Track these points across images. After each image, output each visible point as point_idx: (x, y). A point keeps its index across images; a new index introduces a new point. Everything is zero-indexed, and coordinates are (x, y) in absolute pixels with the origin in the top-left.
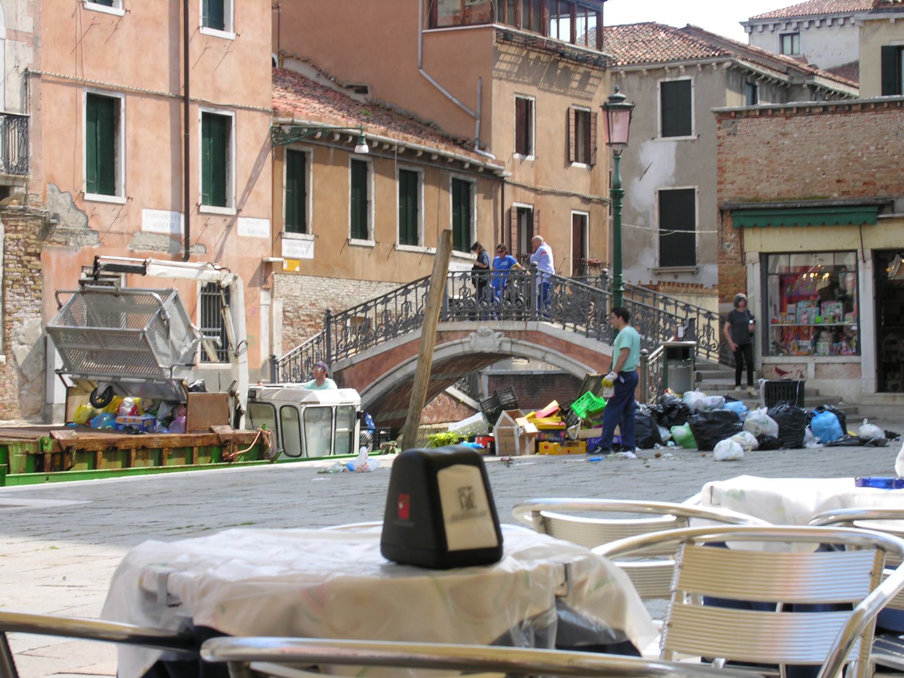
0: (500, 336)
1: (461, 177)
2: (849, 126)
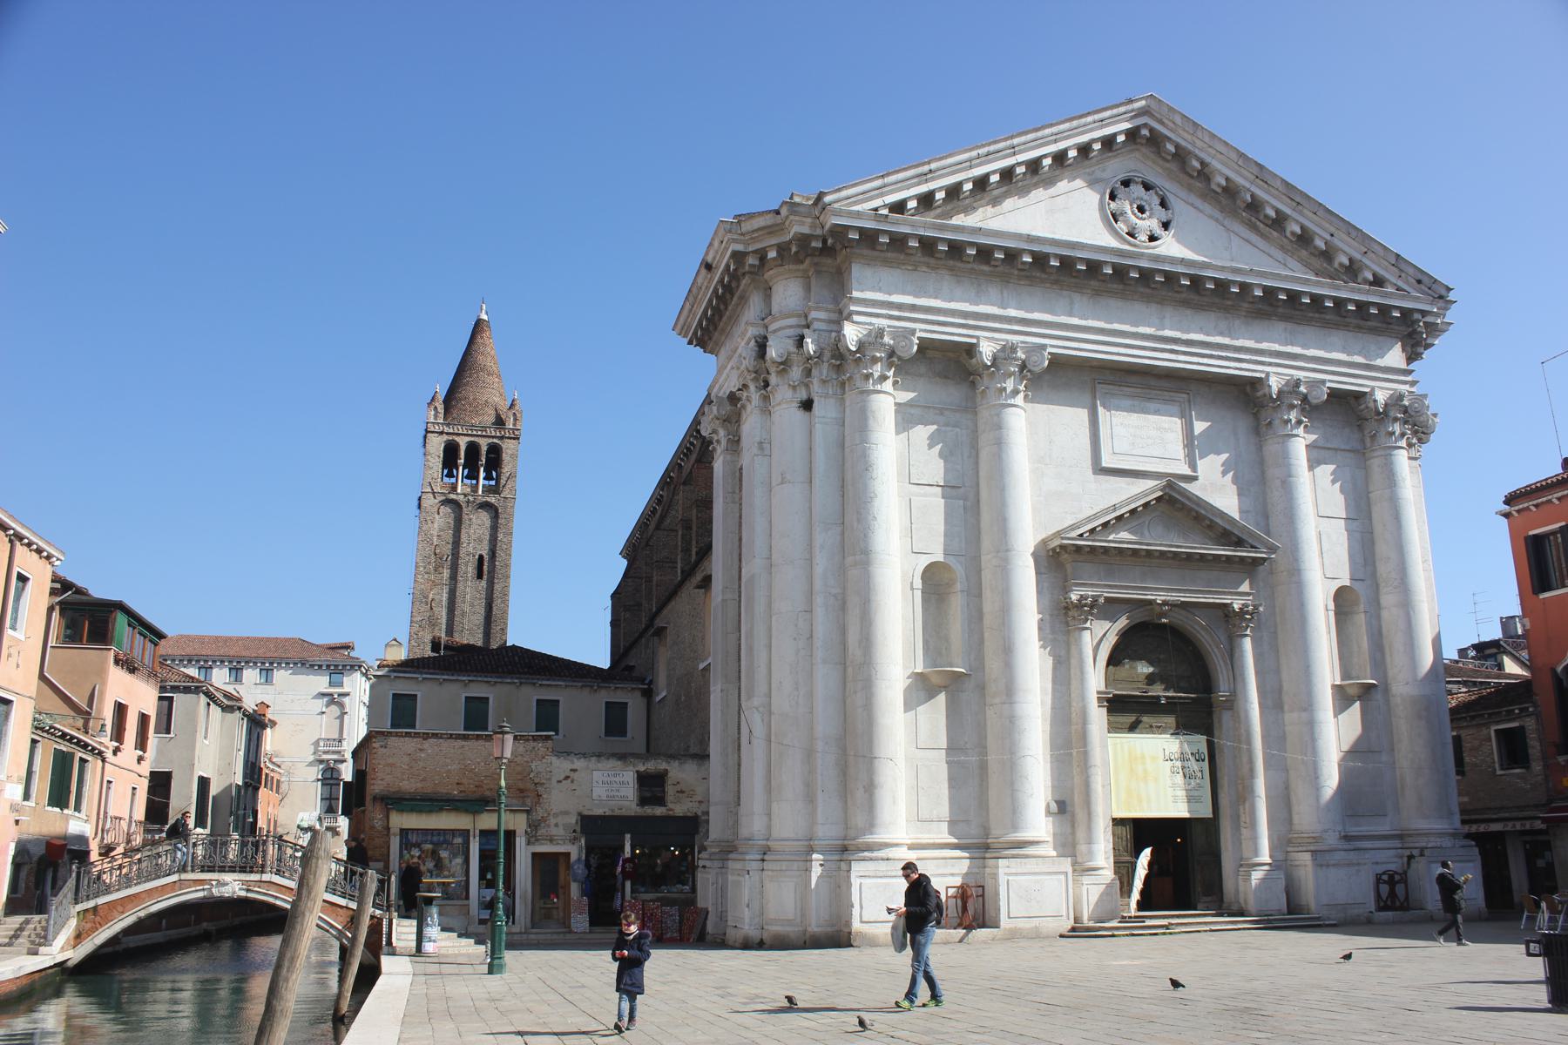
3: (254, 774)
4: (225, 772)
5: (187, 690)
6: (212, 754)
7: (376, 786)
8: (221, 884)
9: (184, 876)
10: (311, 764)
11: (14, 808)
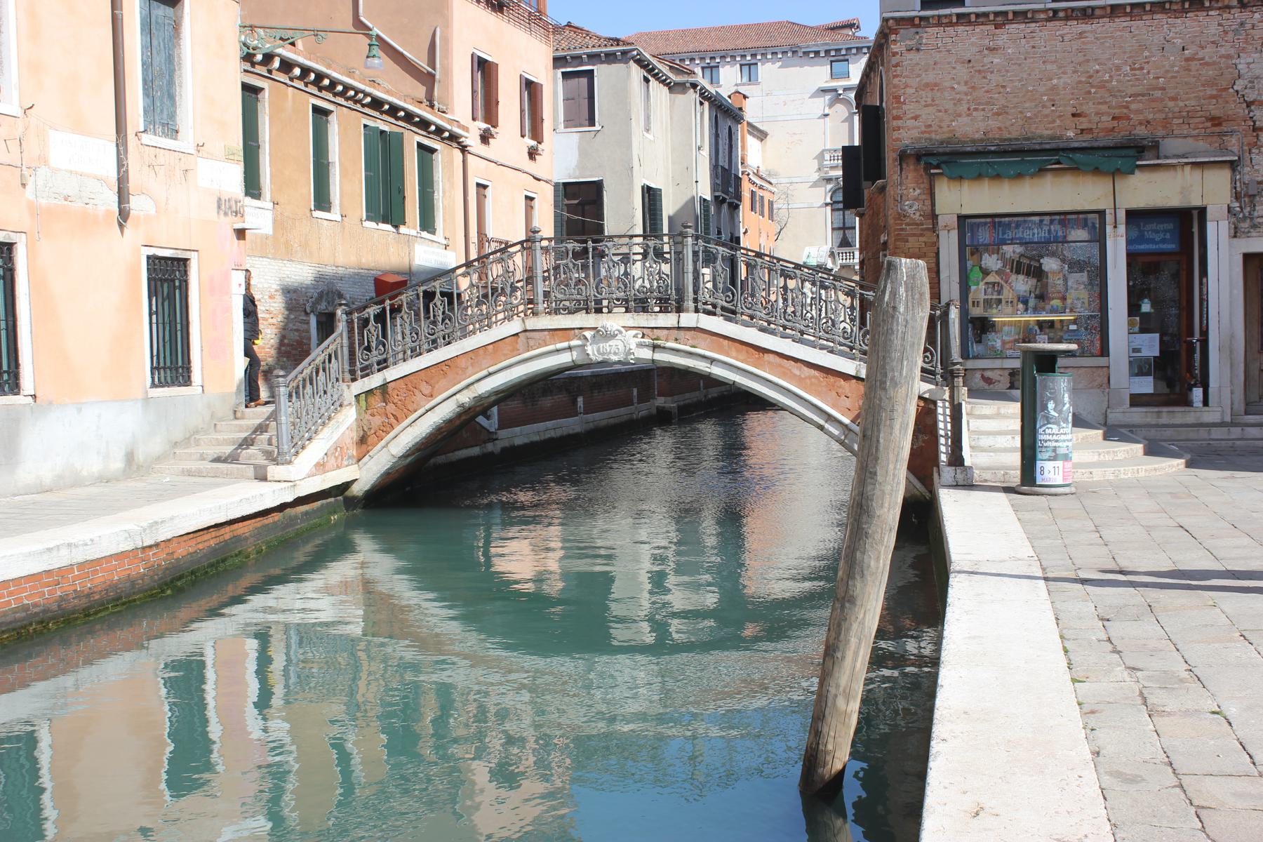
0: (635, 336)
1: (426, 142)
2: (1091, 37)
3: (727, 182)
4: (686, 182)
5: (610, 58)
6: (657, 151)
7: (904, 132)
8: (603, 335)
9: (532, 323)
10: (815, 185)
11: (225, 206)
